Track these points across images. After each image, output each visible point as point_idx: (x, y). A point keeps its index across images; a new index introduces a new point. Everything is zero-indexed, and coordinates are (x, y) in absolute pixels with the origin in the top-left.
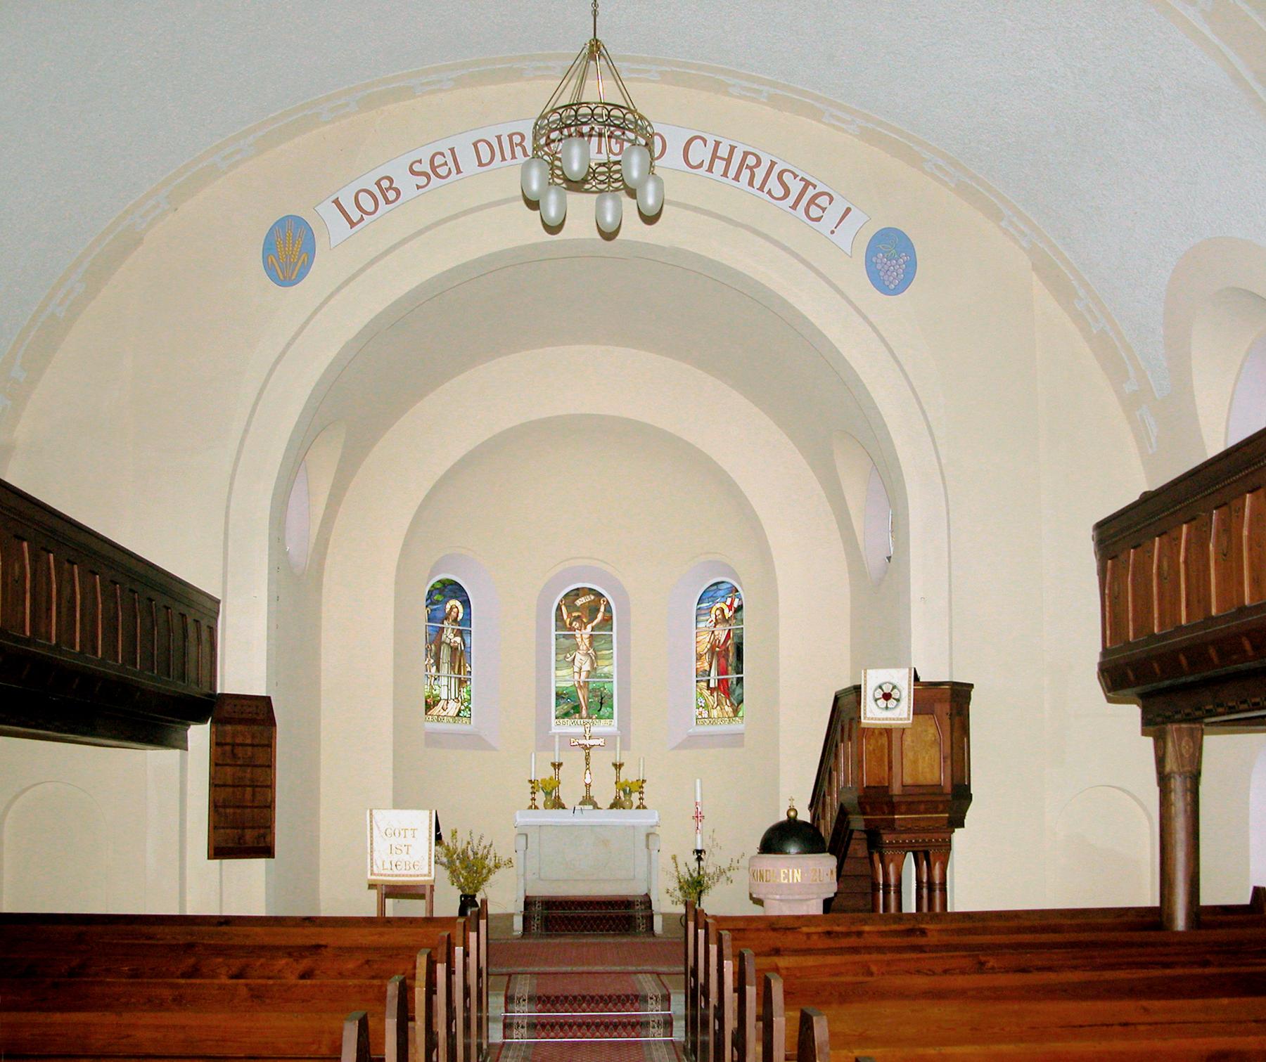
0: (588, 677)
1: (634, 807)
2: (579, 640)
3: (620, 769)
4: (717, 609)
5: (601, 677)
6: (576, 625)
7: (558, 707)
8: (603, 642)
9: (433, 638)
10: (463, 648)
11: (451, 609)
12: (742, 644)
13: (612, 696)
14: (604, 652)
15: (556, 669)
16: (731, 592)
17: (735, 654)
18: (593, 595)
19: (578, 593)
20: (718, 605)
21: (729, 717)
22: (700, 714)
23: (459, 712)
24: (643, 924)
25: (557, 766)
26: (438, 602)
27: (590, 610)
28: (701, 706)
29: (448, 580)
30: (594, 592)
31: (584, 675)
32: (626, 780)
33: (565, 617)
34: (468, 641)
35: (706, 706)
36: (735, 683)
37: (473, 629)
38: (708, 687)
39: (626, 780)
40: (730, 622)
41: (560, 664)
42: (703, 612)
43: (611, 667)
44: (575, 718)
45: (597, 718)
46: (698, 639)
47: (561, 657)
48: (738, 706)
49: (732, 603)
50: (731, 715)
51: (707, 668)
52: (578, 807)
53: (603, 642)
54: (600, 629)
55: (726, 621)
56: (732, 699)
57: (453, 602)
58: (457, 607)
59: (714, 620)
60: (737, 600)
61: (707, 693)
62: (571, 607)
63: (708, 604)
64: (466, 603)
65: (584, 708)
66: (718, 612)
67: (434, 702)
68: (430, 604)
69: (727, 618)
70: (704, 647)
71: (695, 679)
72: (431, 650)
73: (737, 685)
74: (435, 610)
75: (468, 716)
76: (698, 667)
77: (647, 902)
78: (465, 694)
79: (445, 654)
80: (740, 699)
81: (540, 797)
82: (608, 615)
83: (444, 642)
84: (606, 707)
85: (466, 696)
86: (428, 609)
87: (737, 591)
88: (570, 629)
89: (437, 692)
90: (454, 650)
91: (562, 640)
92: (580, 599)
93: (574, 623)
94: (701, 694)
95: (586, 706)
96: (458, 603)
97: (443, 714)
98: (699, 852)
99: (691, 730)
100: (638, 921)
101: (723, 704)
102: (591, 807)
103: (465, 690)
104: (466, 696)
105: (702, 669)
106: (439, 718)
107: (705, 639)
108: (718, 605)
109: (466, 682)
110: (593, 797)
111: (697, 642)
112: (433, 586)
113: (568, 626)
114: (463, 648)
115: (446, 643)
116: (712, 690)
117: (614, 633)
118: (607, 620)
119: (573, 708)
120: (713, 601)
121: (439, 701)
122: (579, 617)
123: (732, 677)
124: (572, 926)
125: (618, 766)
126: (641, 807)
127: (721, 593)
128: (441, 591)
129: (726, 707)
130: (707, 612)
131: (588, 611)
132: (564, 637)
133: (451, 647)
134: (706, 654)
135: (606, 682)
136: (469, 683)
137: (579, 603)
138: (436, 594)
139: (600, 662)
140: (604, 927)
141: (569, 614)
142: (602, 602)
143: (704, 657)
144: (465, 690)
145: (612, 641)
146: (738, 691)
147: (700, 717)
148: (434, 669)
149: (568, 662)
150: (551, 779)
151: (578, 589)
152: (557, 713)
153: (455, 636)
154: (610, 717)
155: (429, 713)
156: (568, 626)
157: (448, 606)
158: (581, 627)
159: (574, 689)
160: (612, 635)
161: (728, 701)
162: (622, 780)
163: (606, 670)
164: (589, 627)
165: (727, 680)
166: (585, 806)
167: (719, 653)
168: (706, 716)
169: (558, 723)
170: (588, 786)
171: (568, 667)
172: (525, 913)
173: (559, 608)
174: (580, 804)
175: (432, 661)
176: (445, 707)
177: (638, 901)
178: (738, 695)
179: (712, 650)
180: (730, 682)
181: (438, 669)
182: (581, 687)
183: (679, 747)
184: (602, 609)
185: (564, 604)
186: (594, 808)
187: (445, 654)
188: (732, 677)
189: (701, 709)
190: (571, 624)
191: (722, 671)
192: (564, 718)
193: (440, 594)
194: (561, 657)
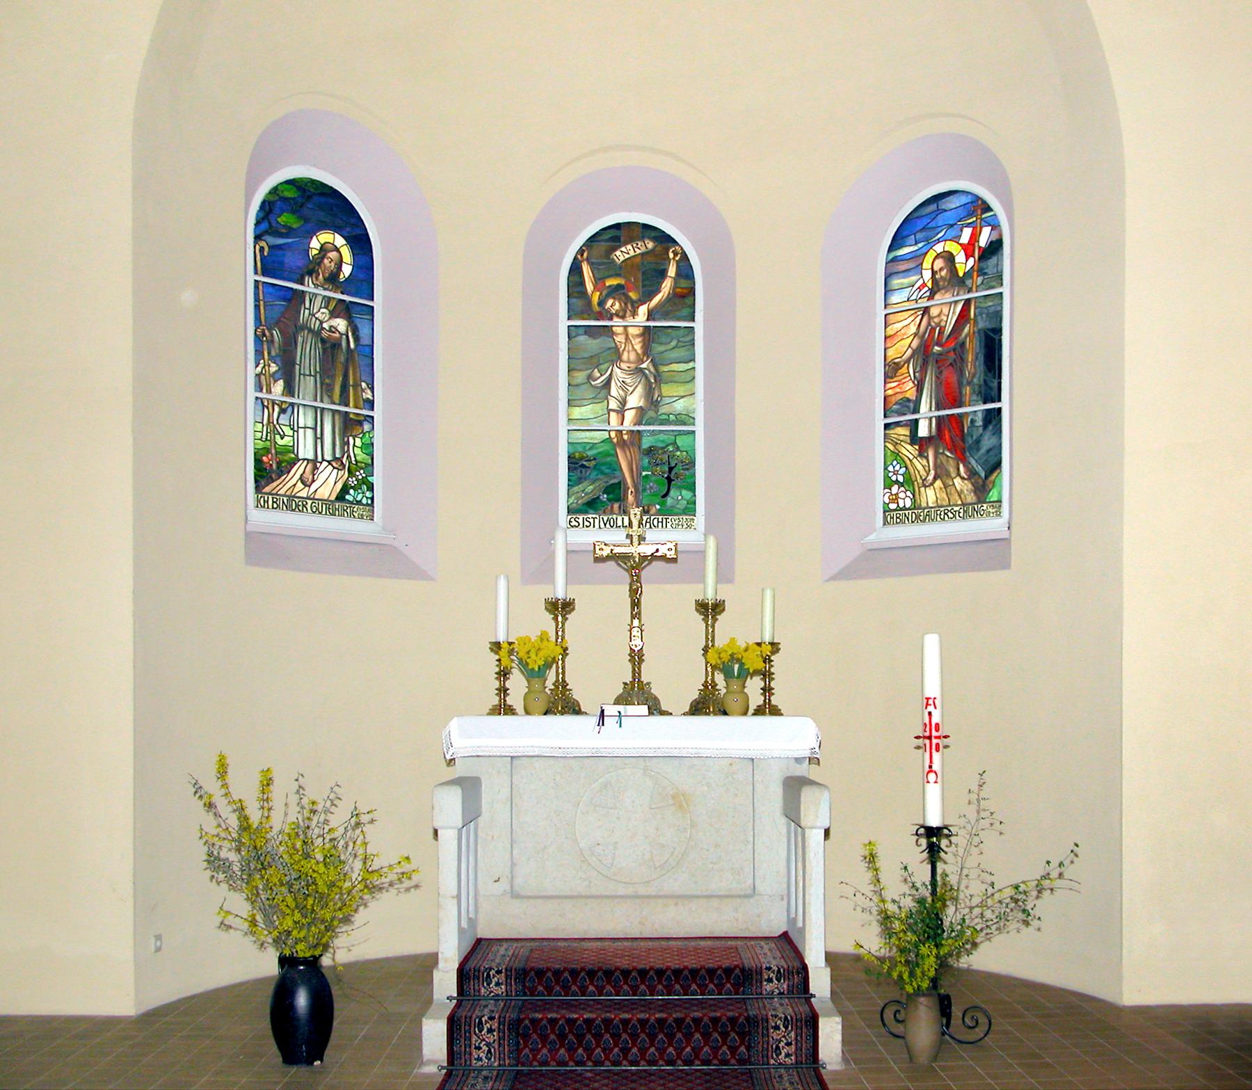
0: (639, 423)
1: (751, 711)
2: (620, 339)
3: (715, 620)
4: (938, 256)
5: (666, 422)
6: (613, 305)
7: (576, 489)
8: (674, 343)
9: (276, 313)
10: (352, 345)
11: (323, 249)
12: (999, 331)
13: (692, 464)
14: (675, 367)
15: (570, 403)
16: (970, 215)
17: (981, 358)
18: (654, 239)
19: (617, 234)
20: (939, 248)
21: (963, 504)
22: (895, 499)
23: (345, 490)
24: (788, 1044)
25: (561, 608)
26: (289, 232)
27: (644, 273)
28: (897, 482)
29: (313, 182)
30: (653, 234)
31: (630, 415)
32: (733, 640)
33: (589, 287)
34: (364, 332)
35: (908, 482)
36: (979, 423)
37: (377, 303)
38: (914, 439)
39: (733, 640)
40: (969, 282)
41: (579, 393)
42: (903, 267)
43: (691, 398)
44: (612, 513)
45: (659, 513)
46: (890, 331)
47: (580, 376)
48: (986, 477)
49: (974, 237)
50: (971, 498)
51: (911, 394)
52: (611, 710)
53: (674, 343)
54: (666, 316)
55: (957, 281)
56: (973, 462)
57: (325, 237)
58: (337, 250)
59: (930, 284)
60: (986, 231)
61: (909, 451)
62: (605, 267)
63: (916, 248)
64: (360, 242)
65: (631, 489)
66: (939, 264)
67: (279, 463)
68: (267, 232)
69: (961, 274)
70: (903, 348)
71: (880, 422)
72: (272, 341)
73: (985, 426)
74: (279, 247)
75: (364, 501)
76: (890, 392)
77: (788, 943)
78: (357, 451)
79: (307, 354)
80: (993, 460)
81: (518, 684)
82: (684, 283)
83: (305, 327)
84: (680, 488)
85: (361, 456)
86: (263, 244)
87: (989, 209)
88: (600, 316)
89: (287, 441)
90: (330, 347)
91: (582, 339)
92: (623, 249)
93: (610, 302)
94: (897, 454)
95: (635, 486)
96: (340, 241)
97: (303, 494)
98: (931, 832)
99: (872, 537)
100: (775, 1035)
101: (949, 475)
102: (644, 709)
103: (358, 442)
104: (361, 456)
105: (899, 397)
106: (293, 504)
107: (908, 328)
108: (939, 248)
109: (360, 423)
110: (649, 684)
111: (886, 338)
112: (274, 191)
113: (597, 308)
114: (352, 345)
115: (310, 330)
116: (922, 444)
117: (699, 325)
118: (683, 296)
119: (607, 490)
120: (927, 240)
121: (293, 463)
122: (619, 287)
123: (975, 409)
124: (589, 1051)
125: (710, 610)
126: (768, 709)
127: (948, 217)
128: (295, 207)
129: (957, 481)
130: (911, 265)
131: (640, 276)
132: (586, 333)
133: (323, 341)
134: (908, 361)
135: (681, 433)
136: (367, 427)
137: (620, 255)
138: (282, 211)
139: (667, 390)
140: (679, 1051)
141: (598, 282)
142: (671, 255)
143: (904, 370)
144: (358, 442)
145: (692, 343)
146: (987, 442)
147: (893, 506)
148: (279, 387)
149: (595, 387)
150: (543, 637)
151: (617, 226)
152: (571, 501)
153: (333, 315)
154: (690, 509)
155: (267, 489)
156: (597, 308)
157: (315, 244)
158: (625, 312)
159: (606, 447)
160: (692, 328)
161: (961, 466)
162: (720, 642)
163: (680, 406)
164: (643, 310)
165: (958, 419)
166: (628, 707)
167: (939, 360)
168: (908, 503)
169: (574, 523)
170: (636, 658)
171: (595, 400)
172: (458, 1005)
173: (575, 269)
174: (618, 701)
175: (274, 368)
176: (308, 476)
177: (769, 969)
178: (988, 451)
179: (923, 353)
180: (967, 423)
181: (289, 390)
182: (623, 444)
183: (847, 573)
184: (672, 271)
185: (587, 259)
186: (651, 713)
187: (307, 354)
188: (975, 409)
189: (895, 489)
190: (601, 303)
191: (948, 397)
192: (586, 512)
193: (293, 212)
194: (580, 376)
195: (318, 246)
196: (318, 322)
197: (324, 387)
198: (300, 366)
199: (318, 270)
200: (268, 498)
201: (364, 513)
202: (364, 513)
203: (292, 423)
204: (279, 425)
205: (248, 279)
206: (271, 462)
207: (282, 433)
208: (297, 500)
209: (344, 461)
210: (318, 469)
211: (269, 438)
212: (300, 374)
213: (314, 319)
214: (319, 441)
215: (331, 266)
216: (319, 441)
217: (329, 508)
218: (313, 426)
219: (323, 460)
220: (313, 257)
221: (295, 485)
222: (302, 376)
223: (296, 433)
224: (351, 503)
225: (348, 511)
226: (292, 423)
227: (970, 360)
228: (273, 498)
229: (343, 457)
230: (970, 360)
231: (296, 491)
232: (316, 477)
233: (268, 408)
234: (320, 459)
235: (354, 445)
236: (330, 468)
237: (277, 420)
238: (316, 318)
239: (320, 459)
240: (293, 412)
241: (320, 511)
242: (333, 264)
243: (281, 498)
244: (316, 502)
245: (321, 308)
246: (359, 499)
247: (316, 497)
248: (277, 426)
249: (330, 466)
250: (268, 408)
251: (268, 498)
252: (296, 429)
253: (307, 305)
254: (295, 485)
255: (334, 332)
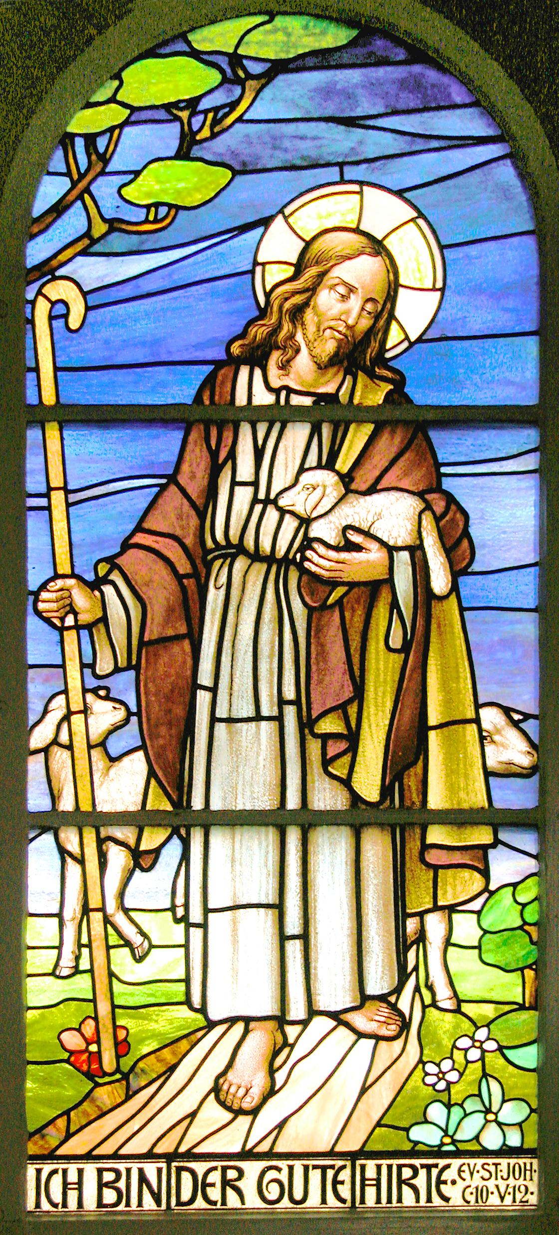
58: (377, 247)
195: (292, 251)
196: (290, 524)
197: (314, 747)
198: (214, 690)
199: (292, 337)
200: (80, 1172)
201: (491, 1184)
202: (491, 1184)
203: (180, 900)
204: (126, 911)
205: (462, 635)
206: (93, 1048)
207: (137, 940)
208: (200, 1168)
209: (404, 1004)
210: (292, 1046)
211: (84, 964)
212: (214, 720)
213: (272, 515)
214: (294, 949)
215: (348, 312)
216: (294, 949)
217: (336, 1182)
218: (272, 899)
219: (312, 1012)
220: (268, 295)
221: (193, 1115)
222: (220, 728)
223: (196, 934)
224: (437, 1152)
225: (421, 1181)
226: (180, 900)
227: (383, 321)
228: (100, 1171)
229: (398, 990)
230: (383, 321)
231: (196, 1132)
232: (280, 1077)
233: (81, 861)
234: (297, 1011)
235: (448, 943)
236: (344, 1036)
237: (121, 895)
238: (283, 512)
239: (297, 1011)
240: (185, 857)
241: (298, 1195)
242: (355, 303)
243: (135, 1167)
244: (283, 1164)
245: (302, 470)
246: (467, 1132)
247: (280, 1148)
248: (120, 919)
249: (342, 1030)
250: (81, 861)
251: (80, 1172)
252: (196, 916)
253: (245, 471)
254: (193, 1115)
255: (358, 548)
